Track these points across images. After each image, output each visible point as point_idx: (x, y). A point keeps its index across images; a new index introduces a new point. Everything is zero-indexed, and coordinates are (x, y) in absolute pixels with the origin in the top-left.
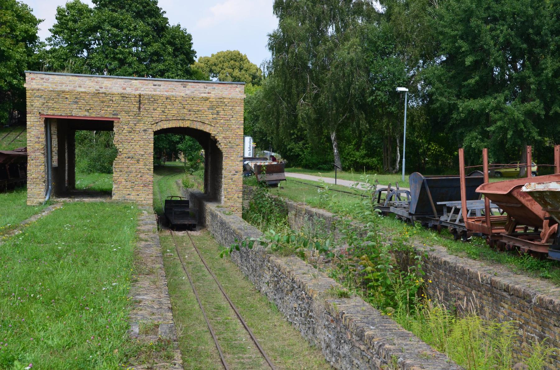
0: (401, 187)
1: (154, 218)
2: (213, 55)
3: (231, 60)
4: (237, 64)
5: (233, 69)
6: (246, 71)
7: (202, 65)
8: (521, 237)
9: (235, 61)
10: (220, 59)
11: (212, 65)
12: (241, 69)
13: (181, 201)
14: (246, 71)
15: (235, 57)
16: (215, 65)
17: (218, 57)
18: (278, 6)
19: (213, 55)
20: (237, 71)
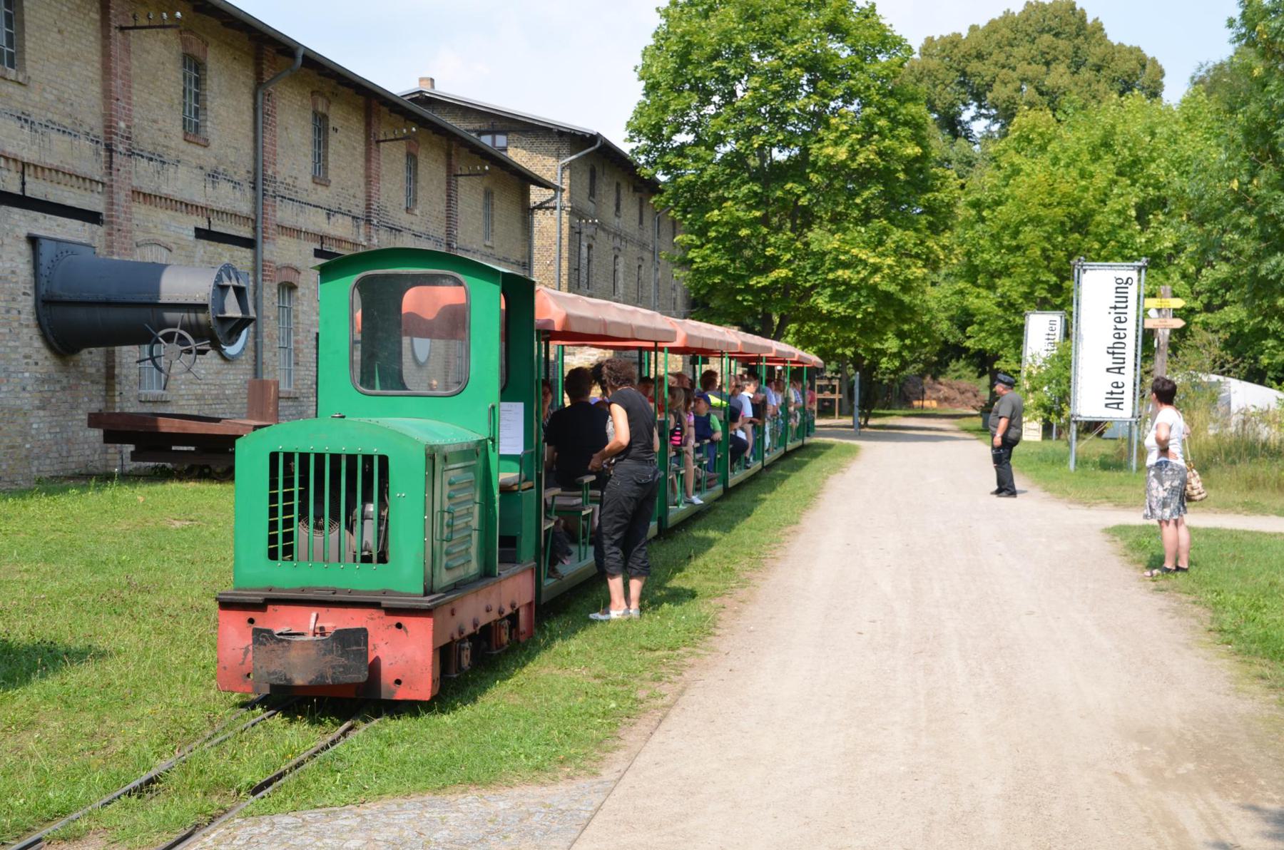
0: (1153, 527)
1: (85, 417)
2: (973, 29)
3: (1042, 32)
4: (1062, 44)
5: (1047, 64)
6: (1098, 69)
7: (934, 63)
8: (251, 344)
9: (1057, 35)
10: (997, 36)
11: (966, 57)
12: (1077, 65)
13: (363, 342)
14: (1098, 69)
15: (1054, 23)
16: (980, 56)
17: (993, 26)
18: (1252, 16)
19: (973, 29)
20: (1062, 68)
